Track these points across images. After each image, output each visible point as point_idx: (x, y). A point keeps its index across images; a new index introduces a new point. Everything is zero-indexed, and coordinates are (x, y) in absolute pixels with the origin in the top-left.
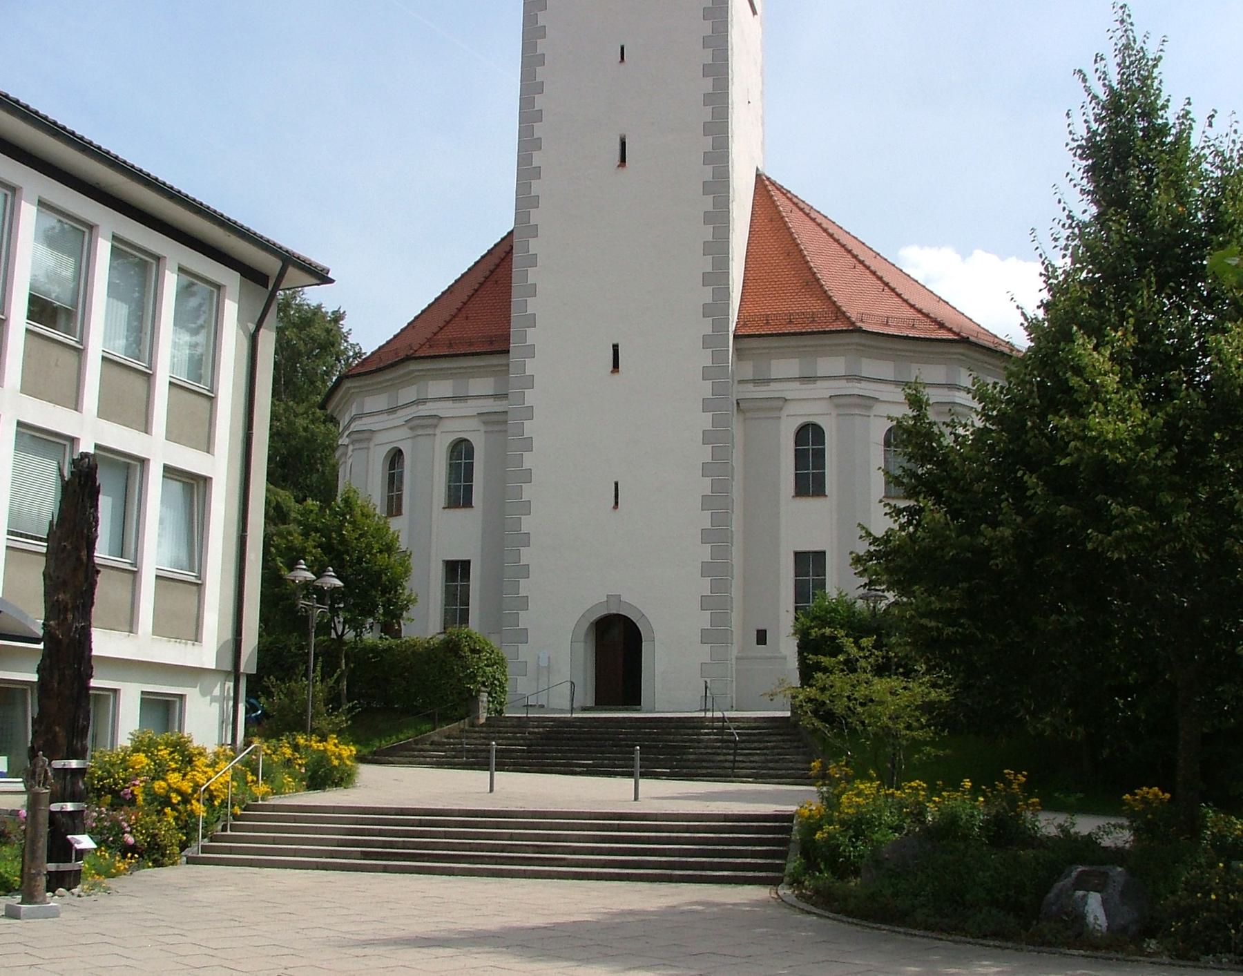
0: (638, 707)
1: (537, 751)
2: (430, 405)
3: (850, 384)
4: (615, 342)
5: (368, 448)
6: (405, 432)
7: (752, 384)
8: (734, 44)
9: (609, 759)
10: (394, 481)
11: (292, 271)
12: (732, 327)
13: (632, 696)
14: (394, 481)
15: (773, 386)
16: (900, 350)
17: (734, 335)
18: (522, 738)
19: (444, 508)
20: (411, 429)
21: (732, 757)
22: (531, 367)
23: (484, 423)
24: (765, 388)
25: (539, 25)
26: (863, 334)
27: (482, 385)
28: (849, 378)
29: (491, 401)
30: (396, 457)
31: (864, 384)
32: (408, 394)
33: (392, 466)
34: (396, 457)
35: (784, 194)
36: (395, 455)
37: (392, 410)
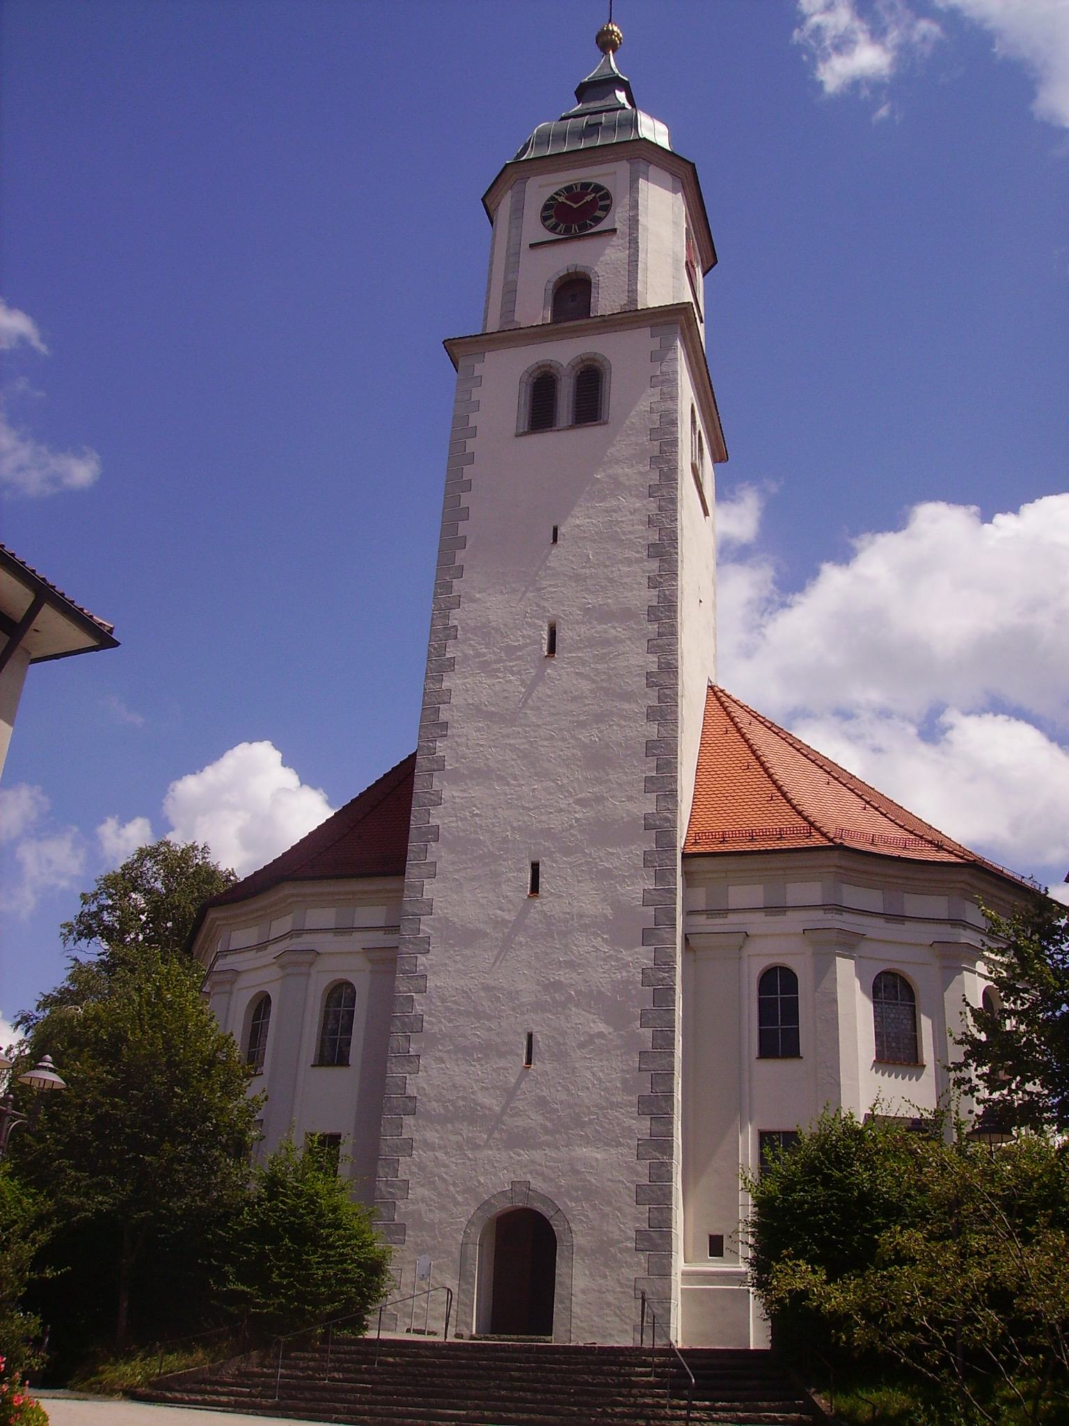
0: (388, 884)
1: (386, 1393)
2: (307, 938)
3: (829, 916)
4: (535, 860)
5: (231, 993)
6: (275, 972)
7: (705, 916)
8: (685, 586)
9: (492, 1409)
10: (256, 1033)
11: (47, 613)
12: (681, 843)
13: (542, 1320)
14: (256, 1033)
15: (732, 918)
16: (890, 876)
17: (683, 853)
18: (367, 1371)
19: (312, 1066)
20: (283, 967)
21: (684, 1412)
22: (430, 889)
23: (370, 961)
24: (721, 921)
25: (470, 426)
26: (846, 853)
27: (370, 915)
28: (825, 907)
29: (380, 934)
30: (262, 1005)
31: (846, 917)
32: (282, 925)
33: (257, 1016)
34: (262, 1005)
35: (742, 707)
36: (259, 1005)
37: (261, 946)
